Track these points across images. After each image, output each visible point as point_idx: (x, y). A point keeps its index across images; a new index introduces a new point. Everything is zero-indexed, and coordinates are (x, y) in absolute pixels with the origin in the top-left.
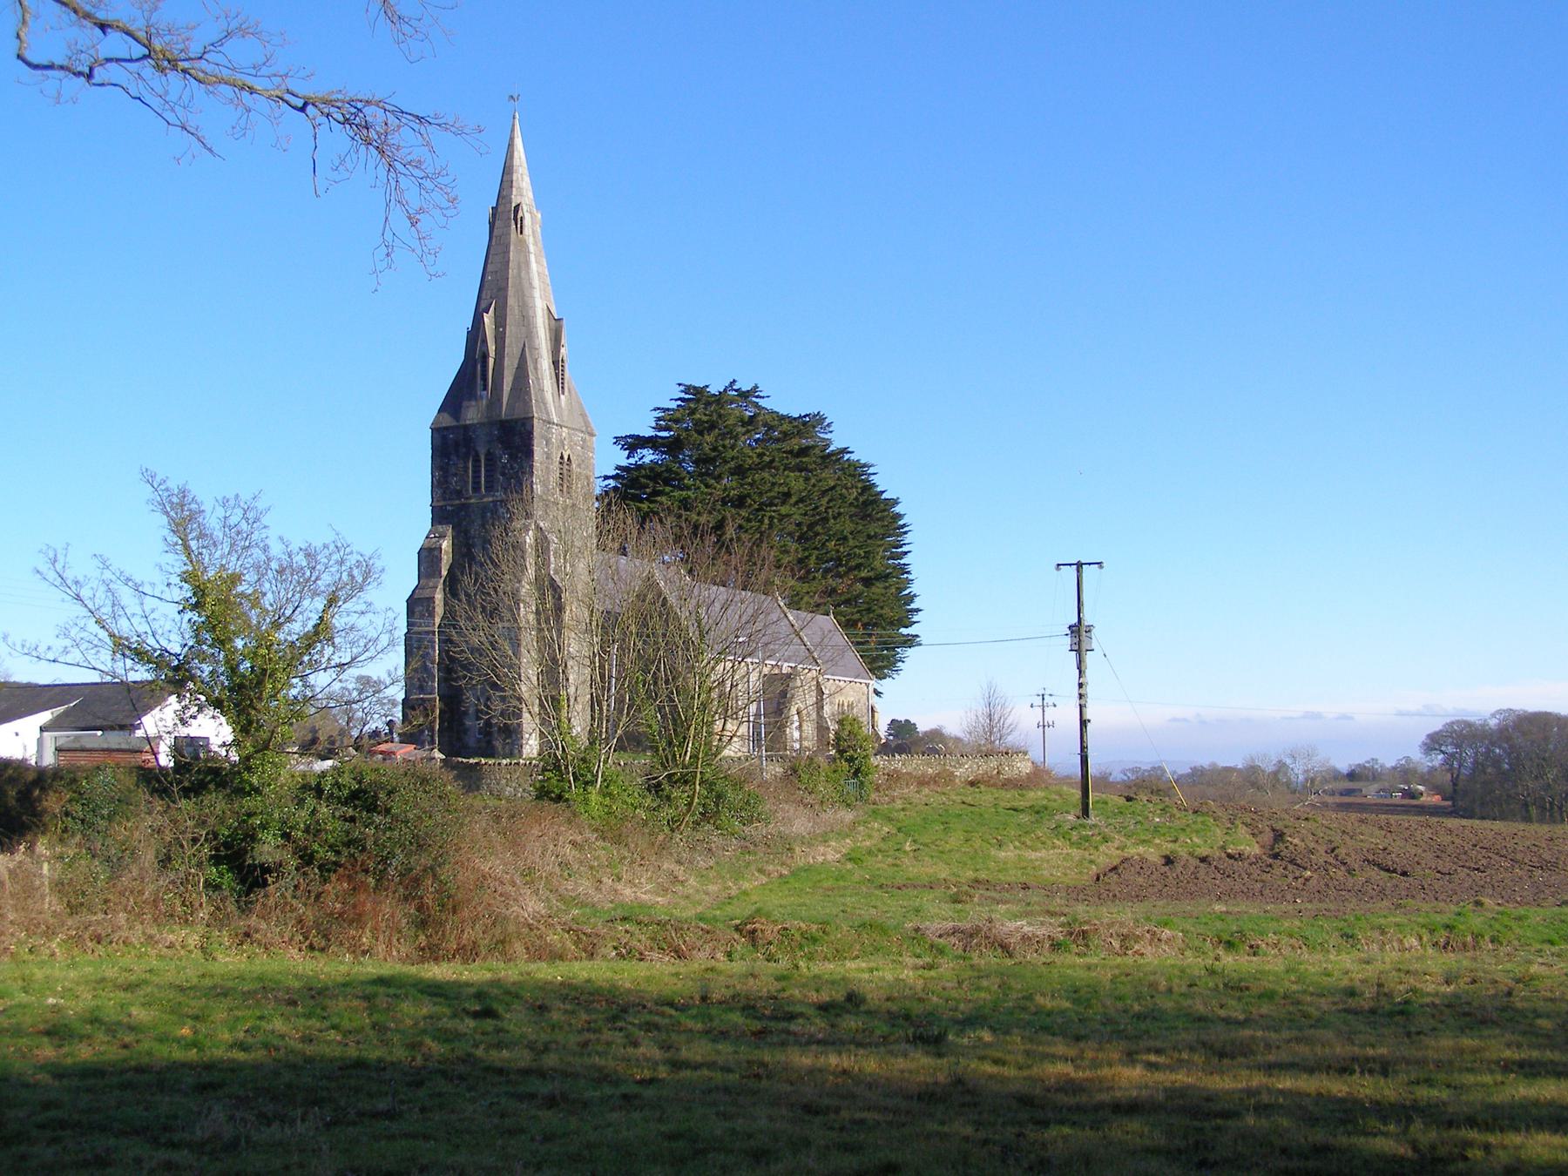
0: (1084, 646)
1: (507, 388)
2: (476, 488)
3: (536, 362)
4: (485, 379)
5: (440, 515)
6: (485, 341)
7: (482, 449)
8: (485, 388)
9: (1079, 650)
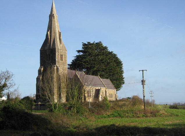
0: (144, 84)
1: (52, 43)
2: (47, 60)
3: (56, 39)
4: (48, 42)
5: (42, 64)
6: (48, 36)
7: (48, 54)
8: (48, 44)
9: (143, 84)
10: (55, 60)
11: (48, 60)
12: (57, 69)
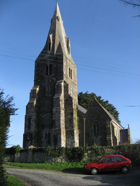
2: (47, 74)
6: (50, 40)
8: (50, 50)
10: (62, 72)
11: (49, 74)
12: (66, 87)
